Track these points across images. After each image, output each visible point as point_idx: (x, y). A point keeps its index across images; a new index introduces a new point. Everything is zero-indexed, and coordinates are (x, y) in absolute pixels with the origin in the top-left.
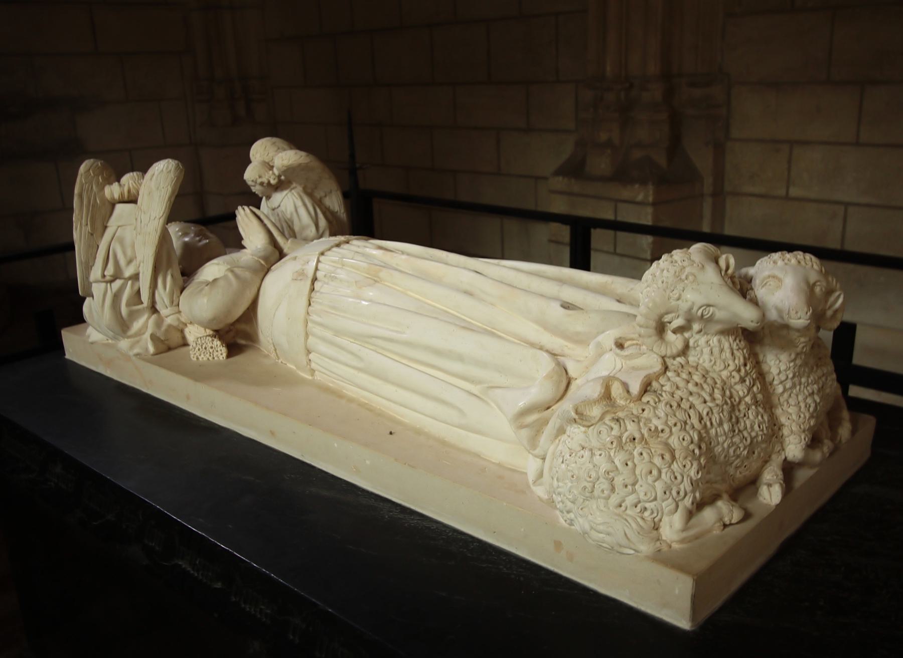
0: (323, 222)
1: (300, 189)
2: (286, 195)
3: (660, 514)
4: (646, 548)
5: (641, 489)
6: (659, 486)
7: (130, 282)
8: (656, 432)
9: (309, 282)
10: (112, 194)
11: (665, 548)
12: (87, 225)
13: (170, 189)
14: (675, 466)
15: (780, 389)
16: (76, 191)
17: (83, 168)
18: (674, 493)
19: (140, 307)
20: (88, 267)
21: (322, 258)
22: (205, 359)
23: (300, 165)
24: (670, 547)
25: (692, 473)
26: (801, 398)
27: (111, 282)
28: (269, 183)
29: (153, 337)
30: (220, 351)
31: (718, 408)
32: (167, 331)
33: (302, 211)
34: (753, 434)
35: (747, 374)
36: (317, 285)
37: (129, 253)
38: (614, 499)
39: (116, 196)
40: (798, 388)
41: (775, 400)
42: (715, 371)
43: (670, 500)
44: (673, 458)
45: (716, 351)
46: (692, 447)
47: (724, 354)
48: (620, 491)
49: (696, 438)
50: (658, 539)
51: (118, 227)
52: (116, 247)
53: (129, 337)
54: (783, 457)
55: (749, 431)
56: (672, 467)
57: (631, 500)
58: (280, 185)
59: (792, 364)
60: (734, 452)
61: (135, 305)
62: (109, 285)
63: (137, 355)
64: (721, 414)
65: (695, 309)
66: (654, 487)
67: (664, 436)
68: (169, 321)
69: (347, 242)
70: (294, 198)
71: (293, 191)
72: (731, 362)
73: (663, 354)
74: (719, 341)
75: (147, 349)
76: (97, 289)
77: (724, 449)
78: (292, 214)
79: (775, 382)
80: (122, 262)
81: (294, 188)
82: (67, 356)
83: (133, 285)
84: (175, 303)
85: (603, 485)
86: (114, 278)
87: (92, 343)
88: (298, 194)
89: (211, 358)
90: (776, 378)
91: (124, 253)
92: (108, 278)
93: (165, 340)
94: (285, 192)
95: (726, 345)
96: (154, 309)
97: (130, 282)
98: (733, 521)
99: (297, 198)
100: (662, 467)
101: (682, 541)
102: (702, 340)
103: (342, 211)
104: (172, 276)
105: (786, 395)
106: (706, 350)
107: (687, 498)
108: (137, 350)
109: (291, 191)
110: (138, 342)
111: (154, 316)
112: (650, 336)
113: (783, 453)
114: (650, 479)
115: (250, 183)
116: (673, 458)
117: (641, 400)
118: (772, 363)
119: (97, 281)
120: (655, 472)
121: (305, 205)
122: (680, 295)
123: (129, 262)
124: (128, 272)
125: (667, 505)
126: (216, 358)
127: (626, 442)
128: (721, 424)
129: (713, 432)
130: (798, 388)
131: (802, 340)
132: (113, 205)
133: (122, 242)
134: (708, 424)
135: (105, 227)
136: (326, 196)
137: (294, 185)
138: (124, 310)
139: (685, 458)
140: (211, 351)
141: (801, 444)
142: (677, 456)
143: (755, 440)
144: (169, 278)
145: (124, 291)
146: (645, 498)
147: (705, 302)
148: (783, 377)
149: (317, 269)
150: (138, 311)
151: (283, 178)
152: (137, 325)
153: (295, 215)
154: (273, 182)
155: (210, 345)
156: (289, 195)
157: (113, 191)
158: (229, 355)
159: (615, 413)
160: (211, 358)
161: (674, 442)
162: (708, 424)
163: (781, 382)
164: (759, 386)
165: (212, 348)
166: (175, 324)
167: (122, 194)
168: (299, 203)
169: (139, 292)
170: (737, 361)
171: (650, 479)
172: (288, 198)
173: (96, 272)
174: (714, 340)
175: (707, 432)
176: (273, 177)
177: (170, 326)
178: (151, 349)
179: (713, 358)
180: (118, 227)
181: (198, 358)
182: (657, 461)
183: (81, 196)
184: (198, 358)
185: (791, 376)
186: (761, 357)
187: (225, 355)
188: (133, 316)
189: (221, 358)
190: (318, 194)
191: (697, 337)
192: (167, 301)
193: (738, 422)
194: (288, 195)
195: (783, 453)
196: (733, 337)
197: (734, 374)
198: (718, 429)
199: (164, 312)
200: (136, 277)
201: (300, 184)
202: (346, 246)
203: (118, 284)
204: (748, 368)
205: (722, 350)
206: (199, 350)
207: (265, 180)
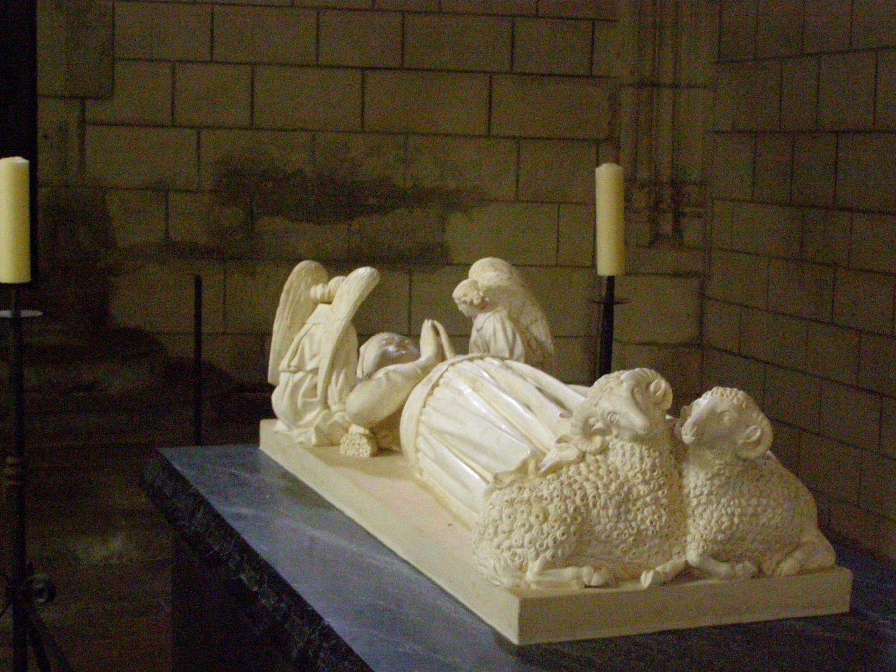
0: (519, 349)
1: (504, 313)
2: (489, 317)
3: (525, 560)
4: (506, 581)
5: (515, 536)
6: (528, 537)
7: (310, 376)
8: (541, 499)
9: (430, 386)
10: (315, 292)
11: (522, 584)
12: (287, 318)
13: (357, 294)
14: (545, 526)
15: (694, 502)
16: (286, 287)
17: (297, 268)
18: (537, 545)
19: (314, 400)
20: (280, 357)
21: (450, 369)
22: (351, 454)
23: (499, 286)
24: (529, 586)
25: (558, 534)
26: (715, 515)
27: (295, 372)
28: (472, 303)
29: (318, 430)
30: (366, 449)
31: (607, 495)
32: (331, 425)
33: (500, 335)
34: (643, 527)
35: (652, 478)
36: (436, 390)
37: (315, 348)
38: (496, 541)
39: (318, 296)
40: (715, 506)
41: (690, 511)
42: (623, 470)
43: (532, 549)
44: (546, 519)
45: (628, 455)
46: (565, 515)
47: (634, 458)
48: (501, 536)
49: (572, 510)
50: (521, 578)
51: (314, 324)
52: (306, 341)
53: (300, 427)
54: (684, 560)
55: (639, 523)
56: (543, 526)
57: (506, 543)
58: (484, 306)
59: (709, 483)
60: (618, 535)
61: (310, 397)
62: (292, 376)
63: (301, 443)
64: (608, 501)
65: (605, 415)
66: (523, 537)
67: (544, 503)
68: (336, 417)
69: (482, 358)
70: (495, 321)
71: (496, 314)
72: (638, 466)
73: (584, 449)
74: (632, 448)
75: (310, 439)
76: (283, 378)
77: (605, 530)
78: (490, 337)
79: (692, 495)
80: (307, 356)
81: (498, 311)
82: (262, 447)
83: (312, 378)
84: (342, 400)
85: (491, 530)
86: (299, 369)
87: (276, 432)
88: (502, 319)
89: (356, 454)
90: (692, 492)
91: (311, 349)
92: (292, 369)
93: (328, 435)
94: (488, 314)
95: (637, 451)
96: (326, 405)
97: (310, 376)
98: (593, 584)
99: (498, 322)
100: (535, 524)
101: (538, 583)
102: (618, 443)
103: (550, 341)
104: (346, 374)
105: (700, 509)
106: (620, 453)
107: (548, 552)
108: (301, 439)
109: (494, 313)
110: (305, 432)
111: (325, 412)
112: (577, 434)
113: (684, 556)
114: (523, 530)
115: (457, 301)
116: (546, 519)
117: (545, 476)
118: (691, 479)
119: (284, 371)
120: (527, 526)
121: (504, 329)
122: (597, 403)
123: (313, 356)
124: (310, 366)
125: (531, 553)
126: (361, 455)
127: (517, 502)
128: (605, 507)
129: (595, 512)
130: (715, 506)
131: (717, 462)
132: (315, 304)
133: (311, 337)
134: (591, 504)
135: (303, 323)
136: (532, 323)
137: (499, 308)
138: (300, 401)
139: (555, 521)
140: (358, 447)
141: (699, 550)
142: (549, 519)
143: (644, 533)
144: (342, 377)
145: (305, 381)
146: (515, 544)
147: (611, 409)
148: (698, 492)
149: (441, 376)
150: (311, 403)
151: (487, 299)
152: (309, 417)
153: (492, 337)
154: (476, 302)
155: (358, 441)
156: (492, 318)
157: (317, 291)
158: (374, 455)
159: (523, 484)
160: (356, 454)
161: (551, 508)
162: (591, 504)
163: (696, 497)
164: (665, 493)
165: (359, 444)
166: (341, 421)
167: (323, 295)
168: (499, 327)
169: (315, 387)
170: (643, 466)
171: (523, 530)
172: (490, 321)
173: (284, 364)
174: (628, 445)
175: (589, 511)
176: (477, 296)
177: (335, 423)
178: (314, 440)
179: (624, 460)
180: (314, 324)
181: (346, 453)
182: (532, 519)
183: (288, 292)
184: (346, 453)
185: (706, 492)
186: (685, 473)
187: (369, 453)
188: (307, 407)
189: (365, 455)
190: (524, 321)
191: (615, 441)
192: (336, 399)
193: (628, 511)
194: (491, 317)
195: (684, 556)
196: (647, 447)
197: (639, 475)
198: (601, 512)
199: (334, 408)
200: (315, 371)
201: (505, 308)
202: (479, 362)
203: (300, 375)
204: (655, 474)
205: (633, 455)
206: (348, 444)
207: (468, 299)
